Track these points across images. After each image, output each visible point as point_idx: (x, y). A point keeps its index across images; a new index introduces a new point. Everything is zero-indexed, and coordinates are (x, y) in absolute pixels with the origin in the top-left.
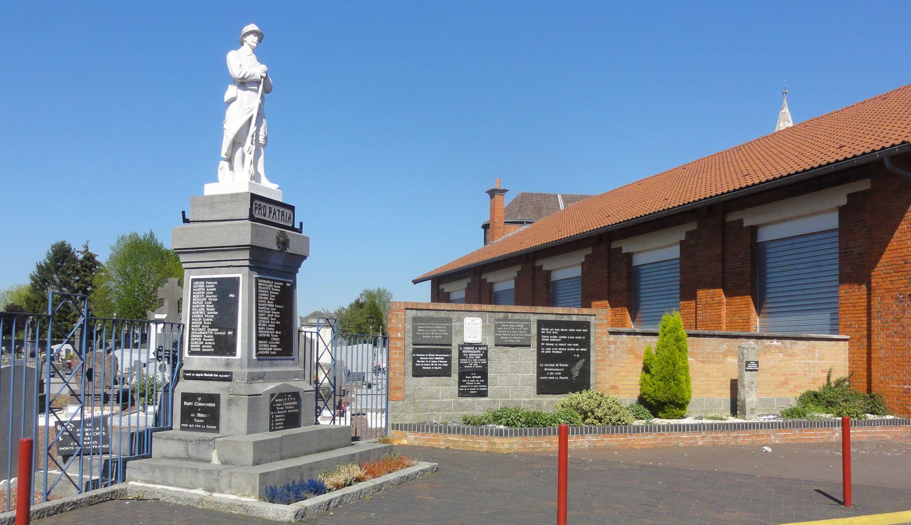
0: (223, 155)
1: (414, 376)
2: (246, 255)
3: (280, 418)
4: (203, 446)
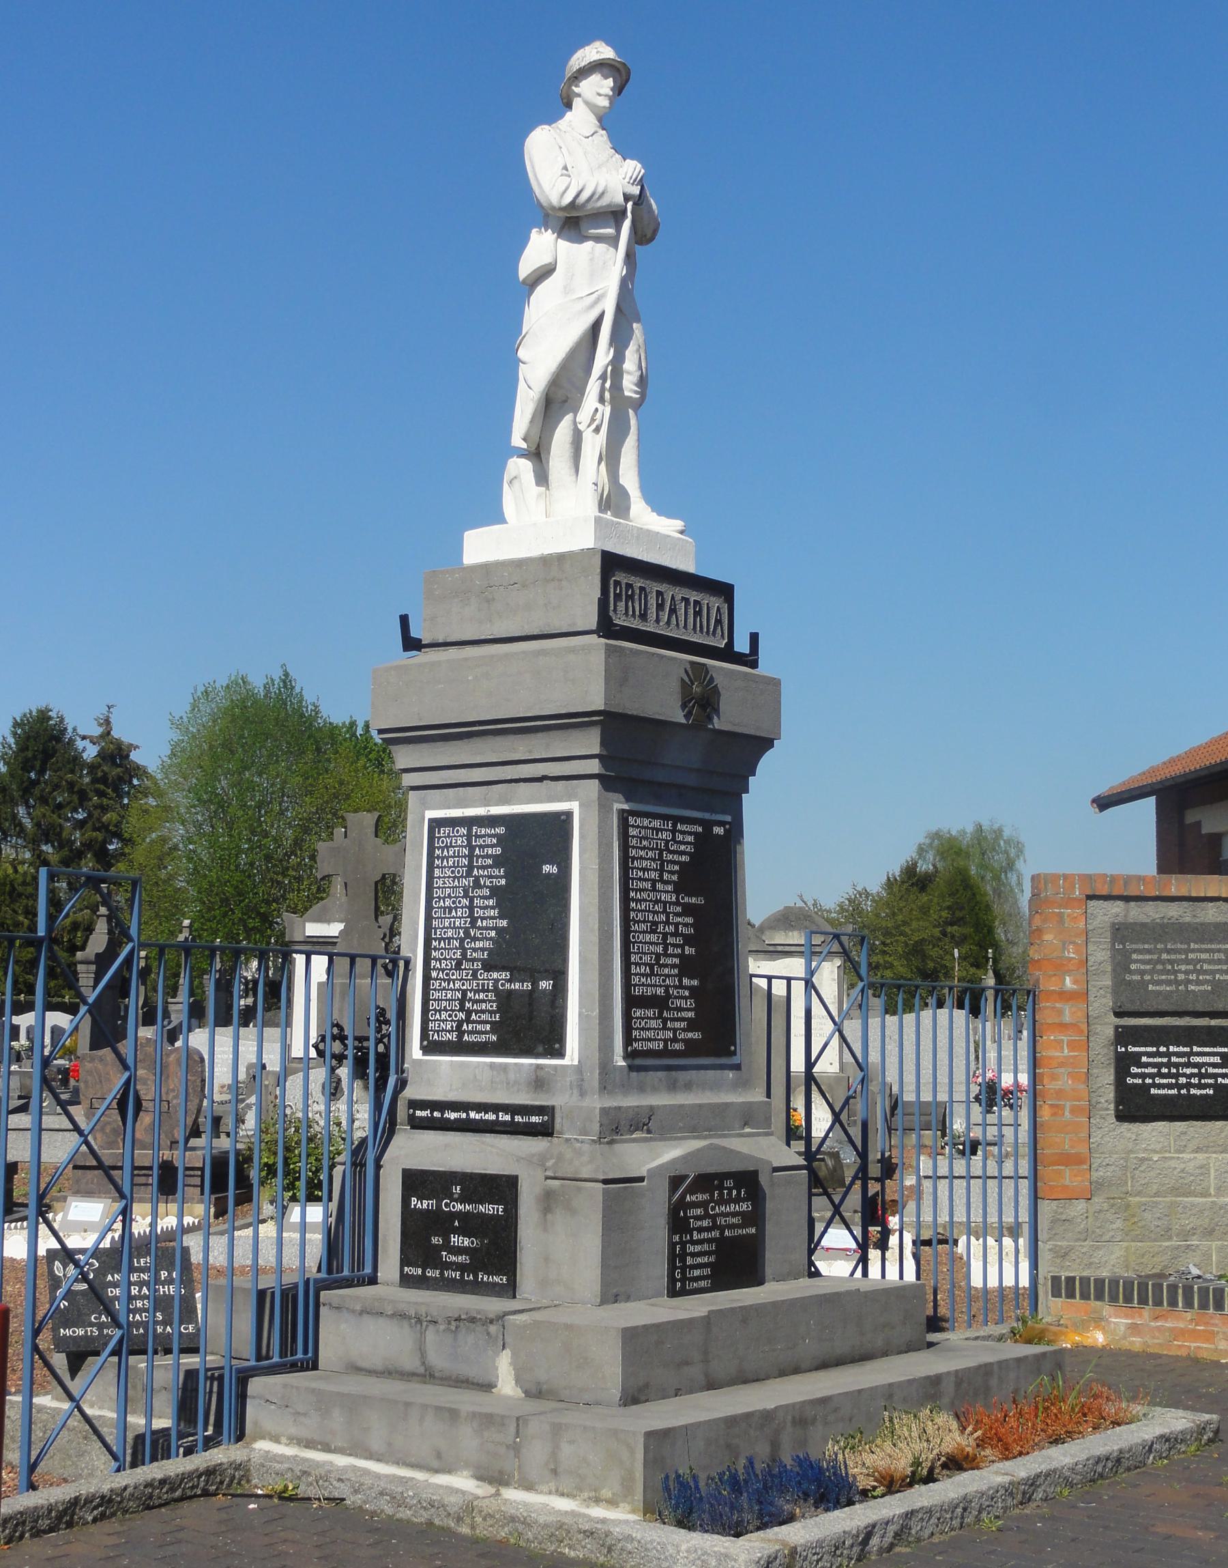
0: (517, 441)
1: (1121, 1117)
2: (591, 741)
3: (700, 1256)
4: (471, 1339)
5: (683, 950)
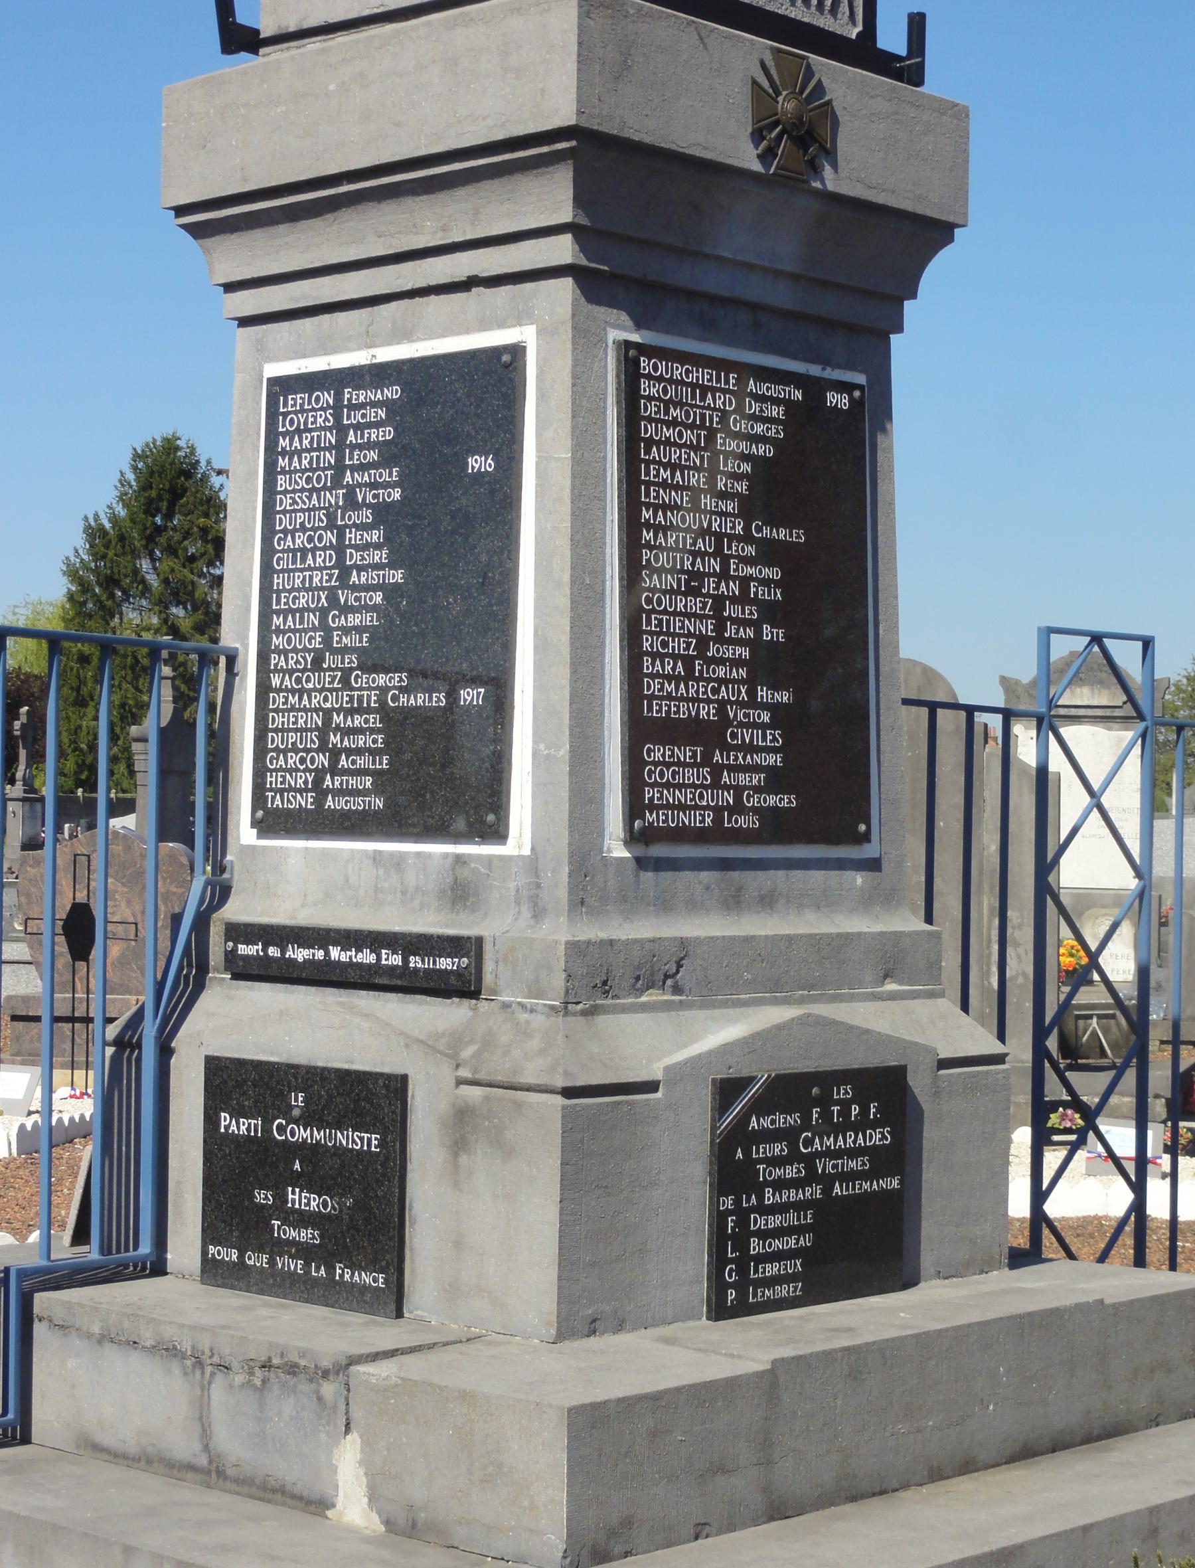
2: (551, 198)
3: (779, 1231)
4: (288, 1406)
5: (759, 632)
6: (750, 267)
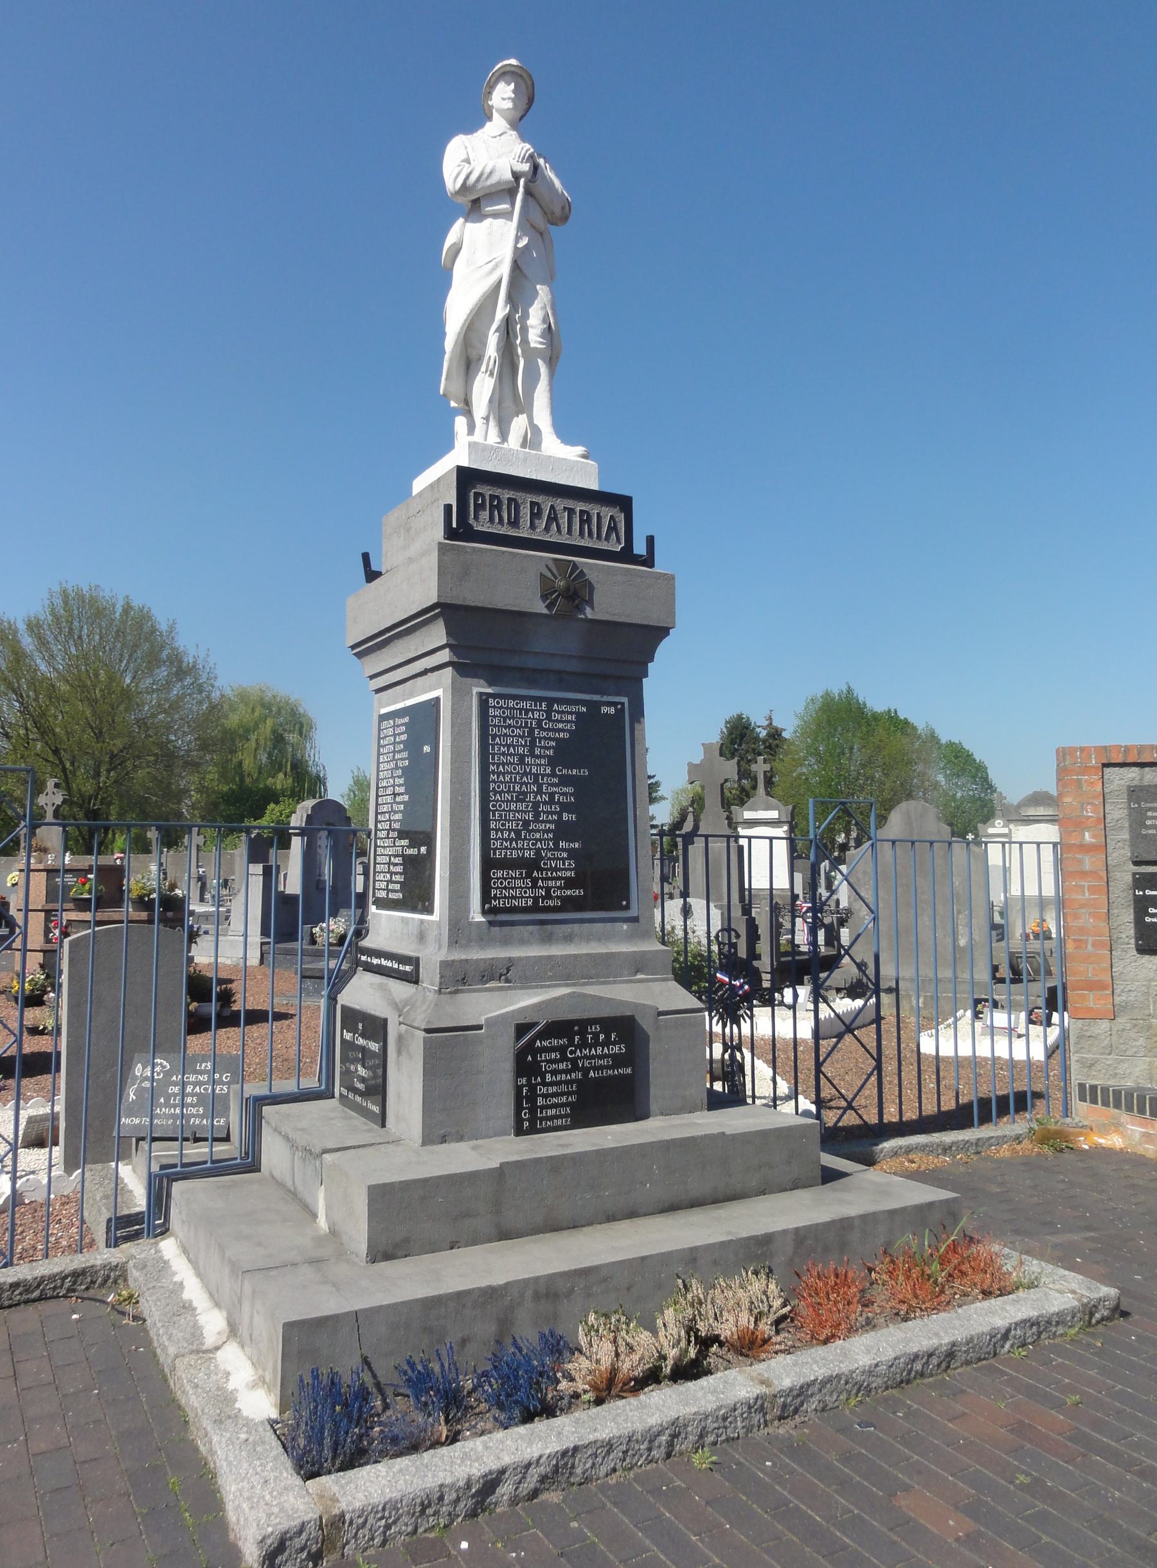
2: (437, 635)
3: (555, 1090)
5: (560, 817)
6: (553, 655)
